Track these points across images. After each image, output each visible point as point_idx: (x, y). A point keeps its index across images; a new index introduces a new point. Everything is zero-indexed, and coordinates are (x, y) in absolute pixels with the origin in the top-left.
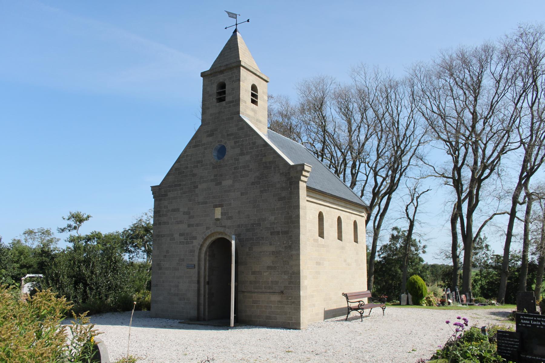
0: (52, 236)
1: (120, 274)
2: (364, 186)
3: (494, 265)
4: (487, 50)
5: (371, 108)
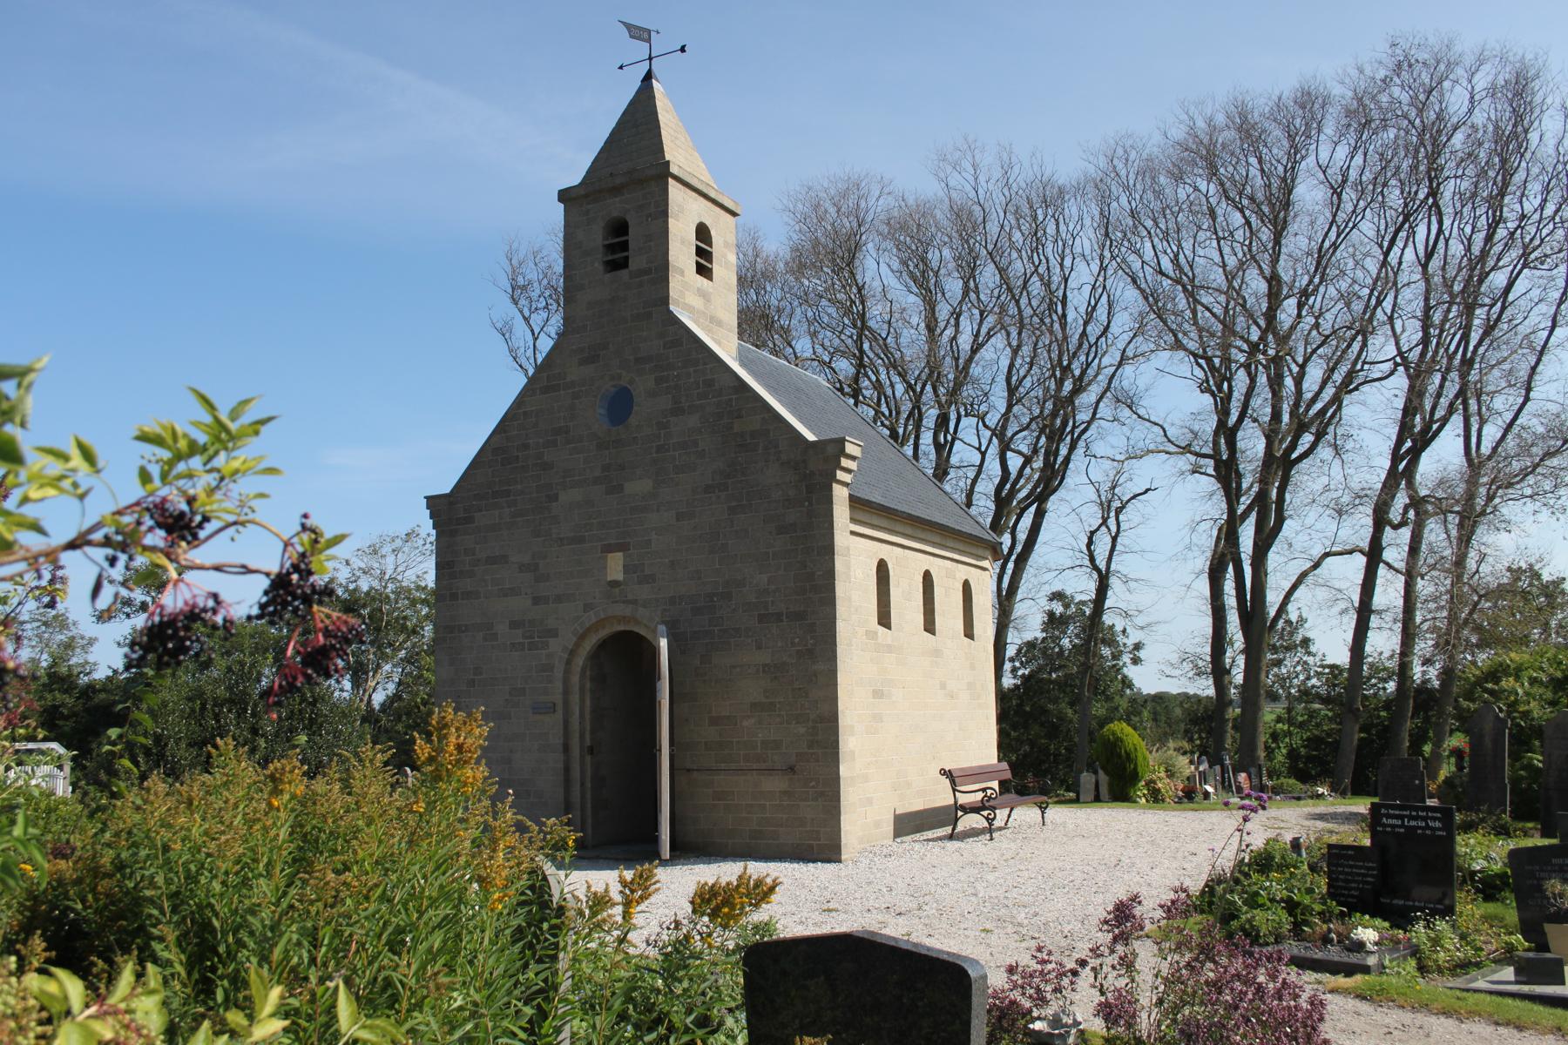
0: (74, 632)
1: (328, 733)
2: (974, 481)
3: (1323, 691)
4: (1310, 103)
5: (987, 254)
